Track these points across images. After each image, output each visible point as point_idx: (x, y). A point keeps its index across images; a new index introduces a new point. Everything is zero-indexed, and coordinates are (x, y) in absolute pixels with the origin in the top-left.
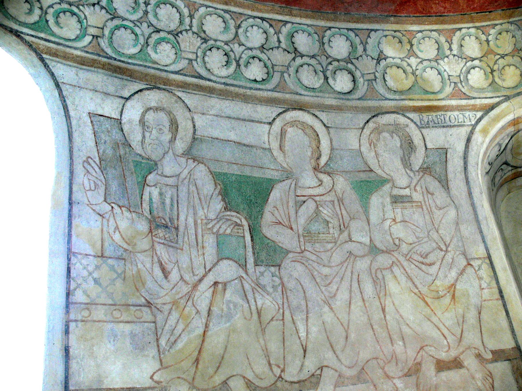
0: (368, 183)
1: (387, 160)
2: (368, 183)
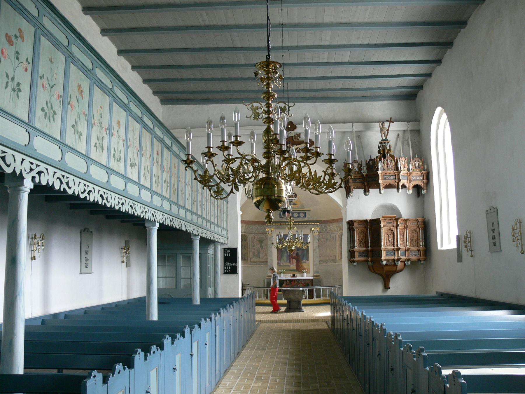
0: (327, 239)
1: (329, 237)
2: (327, 239)
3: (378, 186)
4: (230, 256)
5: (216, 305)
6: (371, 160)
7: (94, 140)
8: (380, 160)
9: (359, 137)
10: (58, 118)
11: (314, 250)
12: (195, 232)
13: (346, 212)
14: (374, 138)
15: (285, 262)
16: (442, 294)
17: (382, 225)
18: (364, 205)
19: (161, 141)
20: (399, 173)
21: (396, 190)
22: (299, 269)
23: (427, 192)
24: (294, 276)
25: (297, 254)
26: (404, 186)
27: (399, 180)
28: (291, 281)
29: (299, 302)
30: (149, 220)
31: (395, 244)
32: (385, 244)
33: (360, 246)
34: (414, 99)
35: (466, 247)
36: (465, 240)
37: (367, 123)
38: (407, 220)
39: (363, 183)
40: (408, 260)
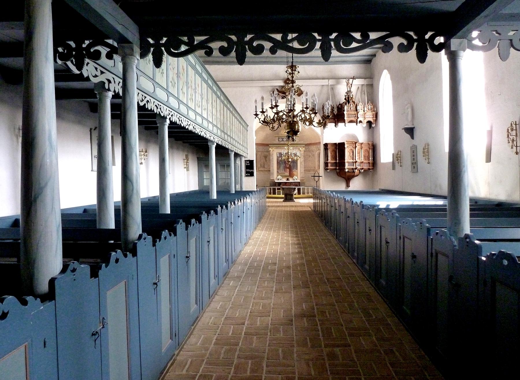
0: (310, 156)
1: (310, 155)
2: (310, 156)
3: (344, 121)
4: (250, 165)
5: (242, 194)
6: (340, 104)
7: (189, 97)
8: (346, 104)
9: (333, 88)
10: (176, 85)
11: (301, 163)
12: (232, 149)
13: (323, 138)
14: (342, 90)
15: (281, 171)
16: (383, 190)
17: (346, 146)
18: (333, 134)
19: (216, 94)
20: (358, 113)
21: (355, 124)
22: (291, 175)
23: (376, 126)
24: (288, 179)
25: (290, 165)
26: (361, 122)
27: (358, 118)
28: (286, 183)
29: (292, 195)
30: (212, 141)
31: (354, 158)
32: (348, 158)
33: (332, 160)
34: (370, 63)
35: (397, 160)
36: (397, 157)
37: (338, 79)
38: (362, 144)
39: (334, 119)
40: (362, 169)
